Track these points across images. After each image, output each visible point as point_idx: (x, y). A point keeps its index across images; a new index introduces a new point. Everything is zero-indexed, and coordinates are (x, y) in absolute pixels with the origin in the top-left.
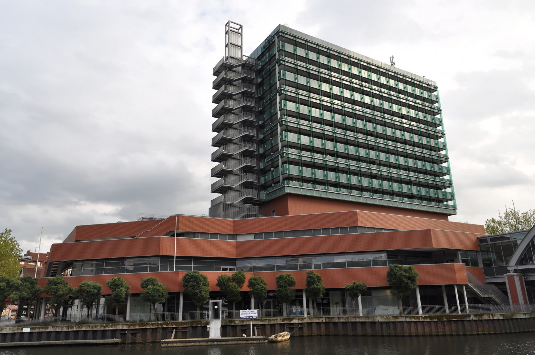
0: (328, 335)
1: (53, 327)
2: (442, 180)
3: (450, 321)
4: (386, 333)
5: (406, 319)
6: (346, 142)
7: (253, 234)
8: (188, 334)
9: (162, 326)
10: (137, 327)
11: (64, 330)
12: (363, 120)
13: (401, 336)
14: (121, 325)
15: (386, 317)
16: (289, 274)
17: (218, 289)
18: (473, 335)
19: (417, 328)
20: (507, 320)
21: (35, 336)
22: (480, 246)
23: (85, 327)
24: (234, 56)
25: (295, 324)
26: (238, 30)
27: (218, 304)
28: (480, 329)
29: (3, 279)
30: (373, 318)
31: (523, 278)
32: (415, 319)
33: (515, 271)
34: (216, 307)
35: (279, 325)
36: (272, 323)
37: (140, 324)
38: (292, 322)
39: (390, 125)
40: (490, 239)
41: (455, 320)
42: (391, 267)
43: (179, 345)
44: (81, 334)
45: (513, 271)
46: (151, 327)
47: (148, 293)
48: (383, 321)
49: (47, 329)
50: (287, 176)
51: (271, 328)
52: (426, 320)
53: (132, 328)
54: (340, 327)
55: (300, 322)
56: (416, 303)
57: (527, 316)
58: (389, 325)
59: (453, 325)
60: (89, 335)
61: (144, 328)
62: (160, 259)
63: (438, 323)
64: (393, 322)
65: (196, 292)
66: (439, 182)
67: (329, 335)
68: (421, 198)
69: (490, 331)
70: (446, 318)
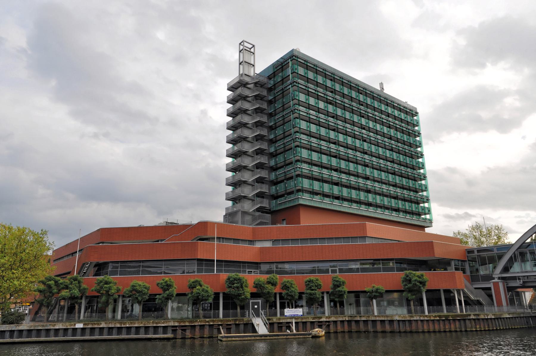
0: (350, 332)
1: (106, 323)
3: (454, 319)
4: (402, 330)
6: (330, 155)
7: (271, 240)
8: (232, 330)
9: (209, 323)
10: (187, 324)
11: (117, 326)
12: (360, 140)
13: (416, 332)
14: (173, 322)
16: (317, 278)
17: (255, 290)
18: (473, 331)
19: (429, 325)
20: (497, 319)
21: (88, 331)
22: (467, 256)
23: (138, 323)
24: (248, 74)
25: (283, 323)
26: (250, 49)
27: (257, 304)
28: (478, 327)
29: (50, 277)
30: (392, 317)
31: (505, 284)
32: (427, 318)
33: (499, 278)
34: (256, 307)
35: (310, 323)
36: (305, 321)
37: (190, 321)
38: (321, 320)
39: (359, 137)
42: (406, 273)
43: (237, 339)
44: (133, 330)
45: (497, 278)
46: (200, 324)
47: (198, 293)
48: (401, 319)
49: (100, 325)
50: (300, 188)
51: (348, 324)
53: (182, 324)
54: (362, 325)
55: (327, 320)
56: (456, 305)
57: (511, 316)
58: (405, 323)
59: (457, 323)
60: (141, 330)
61: (193, 324)
62: (196, 262)
63: (446, 321)
64: (408, 320)
65: (241, 292)
66: (353, 181)
67: (352, 332)
68: (406, 212)
70: (452, 317)
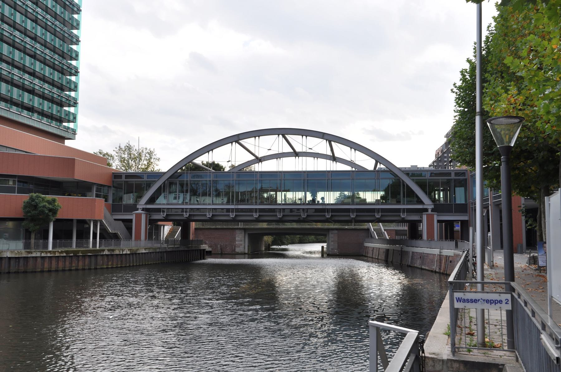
0: (96, 269)
2: (67, 97)
5: (41, 254)
13: (32, 272)
15: (18, 252)
22: (113, 181)
28: (110, 263)
40: (125, 175)
41: (90, 254)
45: (141, 209)
48: (13, 256)
52: (62, 255)
56: (89, 238)
57: (147, 251)
68: (42, 114)
69: (113, 265)
70: (81, 253)
